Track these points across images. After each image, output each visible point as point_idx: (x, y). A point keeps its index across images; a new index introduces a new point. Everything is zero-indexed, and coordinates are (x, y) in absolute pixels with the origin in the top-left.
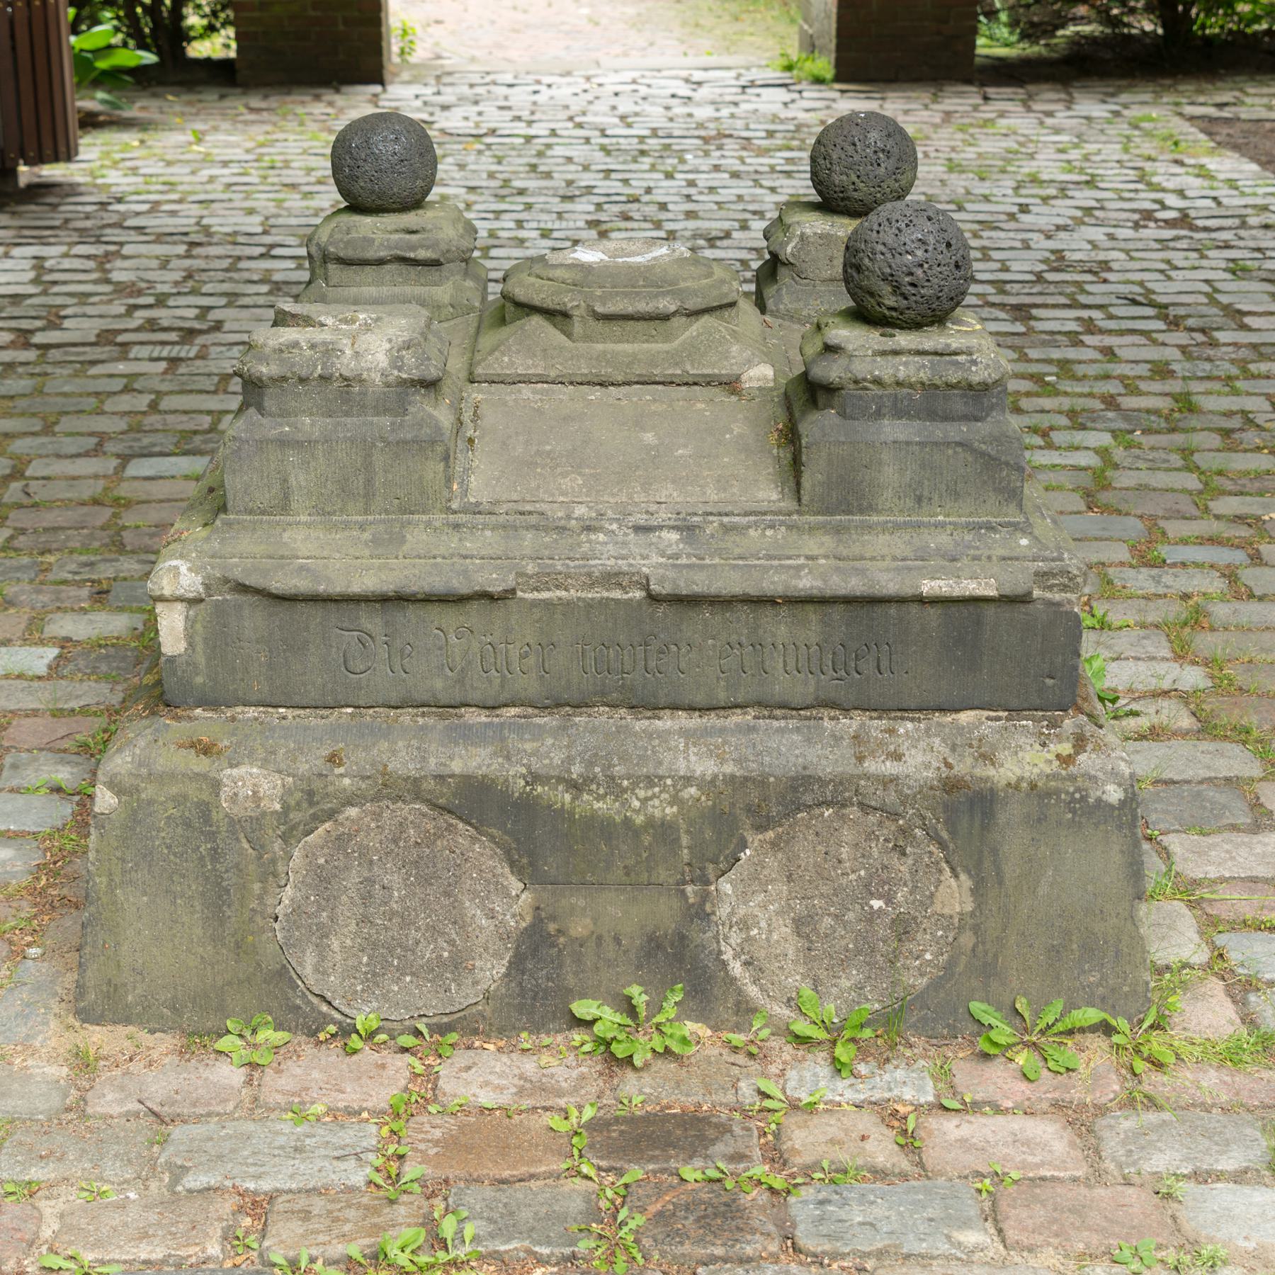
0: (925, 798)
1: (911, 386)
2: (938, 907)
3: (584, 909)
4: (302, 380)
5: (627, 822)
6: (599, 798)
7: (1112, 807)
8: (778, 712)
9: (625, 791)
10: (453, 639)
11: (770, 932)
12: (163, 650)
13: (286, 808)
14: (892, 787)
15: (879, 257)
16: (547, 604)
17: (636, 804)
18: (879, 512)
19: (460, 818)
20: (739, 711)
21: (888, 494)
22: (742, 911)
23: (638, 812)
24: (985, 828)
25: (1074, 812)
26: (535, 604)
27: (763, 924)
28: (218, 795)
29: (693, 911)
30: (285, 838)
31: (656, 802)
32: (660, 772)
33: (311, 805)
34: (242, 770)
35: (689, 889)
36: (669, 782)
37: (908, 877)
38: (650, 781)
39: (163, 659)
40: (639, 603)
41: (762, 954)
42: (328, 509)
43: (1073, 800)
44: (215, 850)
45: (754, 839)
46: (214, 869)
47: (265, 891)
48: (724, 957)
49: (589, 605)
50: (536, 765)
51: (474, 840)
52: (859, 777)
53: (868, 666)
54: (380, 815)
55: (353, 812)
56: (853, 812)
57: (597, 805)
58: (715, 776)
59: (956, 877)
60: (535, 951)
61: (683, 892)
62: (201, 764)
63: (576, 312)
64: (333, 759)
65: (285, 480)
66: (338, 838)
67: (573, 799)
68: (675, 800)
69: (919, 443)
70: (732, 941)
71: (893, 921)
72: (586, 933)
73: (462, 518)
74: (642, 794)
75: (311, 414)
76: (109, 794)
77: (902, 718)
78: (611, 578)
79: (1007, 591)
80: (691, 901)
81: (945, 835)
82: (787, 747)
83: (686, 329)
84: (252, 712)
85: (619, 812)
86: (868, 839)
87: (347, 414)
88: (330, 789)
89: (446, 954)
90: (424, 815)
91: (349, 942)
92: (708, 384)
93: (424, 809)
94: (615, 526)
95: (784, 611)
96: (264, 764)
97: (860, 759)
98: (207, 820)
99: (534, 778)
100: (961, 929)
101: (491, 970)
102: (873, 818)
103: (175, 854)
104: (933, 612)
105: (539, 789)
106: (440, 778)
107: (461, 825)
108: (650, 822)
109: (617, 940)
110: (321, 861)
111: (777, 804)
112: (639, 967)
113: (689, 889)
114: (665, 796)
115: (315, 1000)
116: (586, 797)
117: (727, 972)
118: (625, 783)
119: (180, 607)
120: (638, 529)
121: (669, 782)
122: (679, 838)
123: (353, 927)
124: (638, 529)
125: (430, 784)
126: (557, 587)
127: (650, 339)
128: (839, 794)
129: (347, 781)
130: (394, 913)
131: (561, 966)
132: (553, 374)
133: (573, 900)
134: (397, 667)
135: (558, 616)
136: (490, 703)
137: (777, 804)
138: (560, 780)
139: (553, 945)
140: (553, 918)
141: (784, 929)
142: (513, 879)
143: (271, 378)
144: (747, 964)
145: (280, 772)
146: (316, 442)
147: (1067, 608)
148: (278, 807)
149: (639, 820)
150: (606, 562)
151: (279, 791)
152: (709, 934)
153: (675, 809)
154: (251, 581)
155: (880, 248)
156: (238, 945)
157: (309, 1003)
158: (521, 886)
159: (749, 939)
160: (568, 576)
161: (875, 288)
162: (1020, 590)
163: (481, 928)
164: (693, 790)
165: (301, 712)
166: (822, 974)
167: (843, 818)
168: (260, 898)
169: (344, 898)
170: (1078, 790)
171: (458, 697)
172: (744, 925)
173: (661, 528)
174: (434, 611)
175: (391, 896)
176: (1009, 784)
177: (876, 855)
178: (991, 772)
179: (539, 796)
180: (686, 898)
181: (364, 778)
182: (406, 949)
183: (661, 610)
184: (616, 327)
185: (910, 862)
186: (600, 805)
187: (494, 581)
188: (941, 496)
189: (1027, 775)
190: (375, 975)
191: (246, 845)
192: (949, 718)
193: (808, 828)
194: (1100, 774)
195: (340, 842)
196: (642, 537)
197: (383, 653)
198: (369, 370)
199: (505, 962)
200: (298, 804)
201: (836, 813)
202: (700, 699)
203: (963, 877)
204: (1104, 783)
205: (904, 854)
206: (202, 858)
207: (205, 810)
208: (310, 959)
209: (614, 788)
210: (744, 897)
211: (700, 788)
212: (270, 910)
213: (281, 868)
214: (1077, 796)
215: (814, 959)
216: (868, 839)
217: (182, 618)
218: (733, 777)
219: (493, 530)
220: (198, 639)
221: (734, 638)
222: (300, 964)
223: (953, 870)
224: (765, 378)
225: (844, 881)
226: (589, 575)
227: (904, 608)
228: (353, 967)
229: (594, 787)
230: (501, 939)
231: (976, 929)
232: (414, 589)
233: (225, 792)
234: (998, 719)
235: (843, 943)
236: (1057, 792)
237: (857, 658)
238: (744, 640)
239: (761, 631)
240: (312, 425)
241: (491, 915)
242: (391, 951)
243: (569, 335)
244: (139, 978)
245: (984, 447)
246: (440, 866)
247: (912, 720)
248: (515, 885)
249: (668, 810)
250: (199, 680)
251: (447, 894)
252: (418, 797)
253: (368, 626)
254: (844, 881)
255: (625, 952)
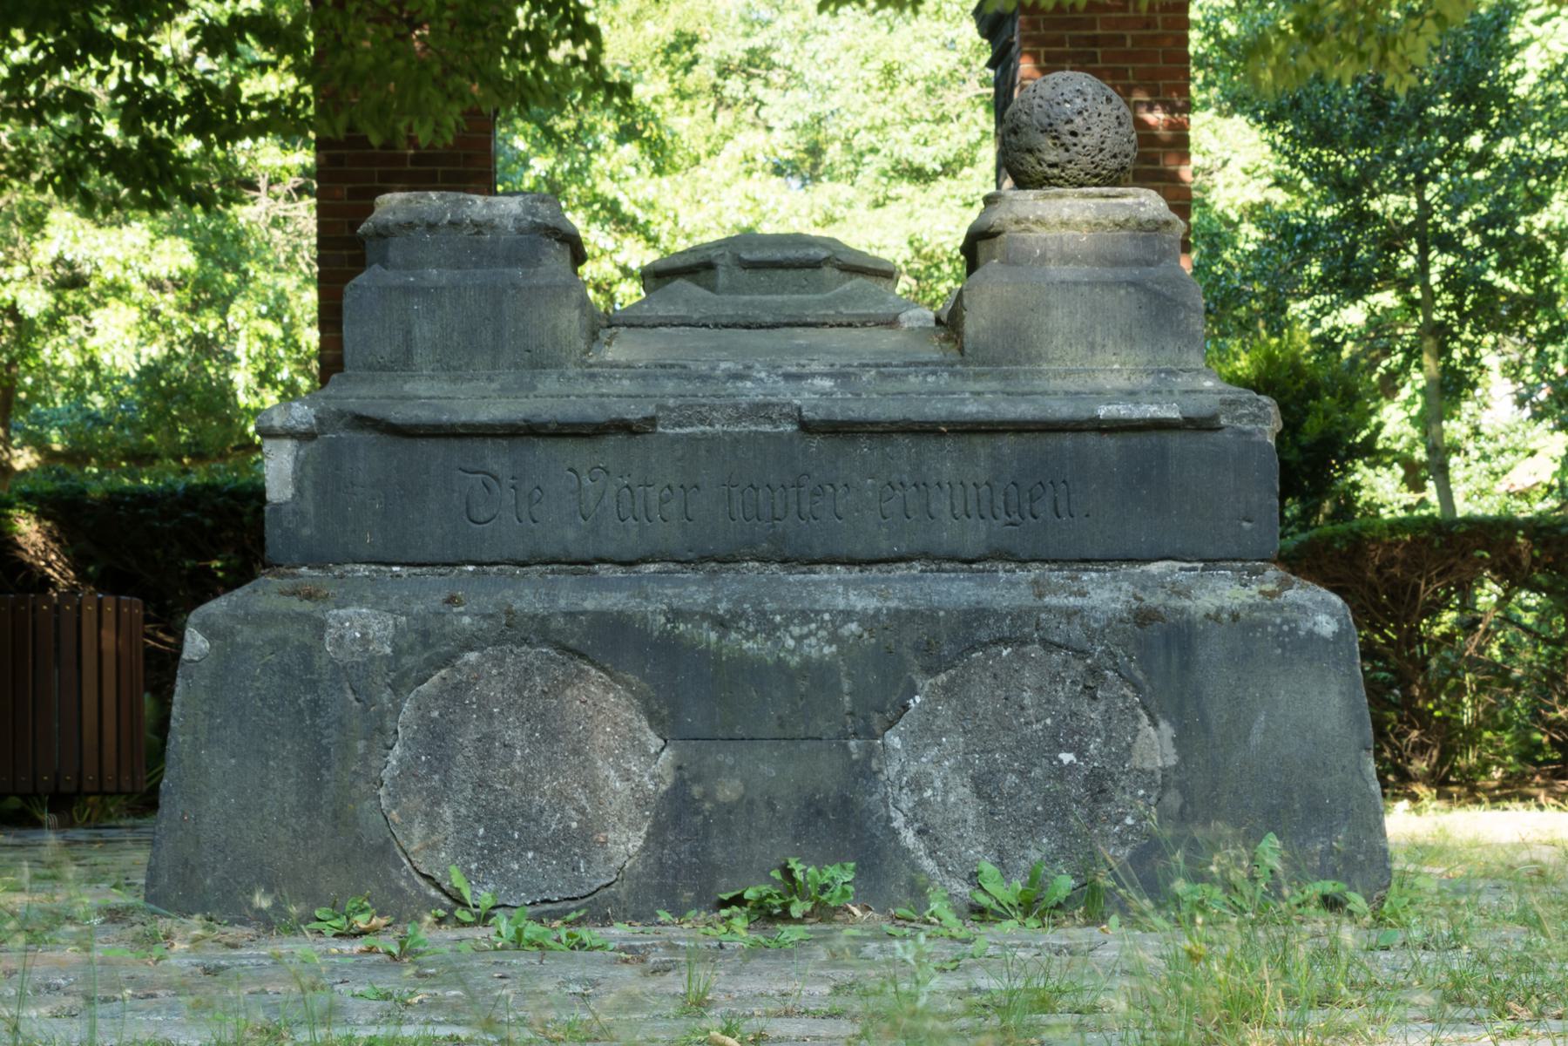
0: (1114, 632)
1: (1077, 226)
2: (1136, 761)
3: (732, 768)
4: (431, 227)
5: (781, 664)
6: (750, 636)
7: (1325, 640)
8: (947, 566)
9: (776, 627)
10: (586, 482)
11: (946, 793)
12: (269, 496)
13: (398, 652)
14: (1077, 620)
15: (1036, 109)
16: (691, 438)
17: (791, 643)
18: (1049, 362)
19: (592, 663)
20: (903, 565)
21: (1058, 340)
22: (913, 768)
23: (792, 652)
24: (1186, 666)
25: (1283, 646)
26: (677, 439)
27: (938, 784)
28: (322, 638)
29: (857, 769)
30: (395, 687)
31: (813, 641)
32: (817, 607)
33: (429, 648)
34: (351, 611)
35: (852, 743)
36: (827, 617)
37: (1100, 725)
38: (805, 616)
39: (267, 508)
40: (791, 436)
41: (938, 820)
42: (454, 363)
43: (1281, 633)
44: (316, 702)
45: (925, 683)
46: (313, 725)
47: (369, 750)
48: (895, 824)
49: (736, 440)
50: (676, 603)
51: (607, 689)
52: (1040, 610)
53: (1044, 508)
54: (503, 660)
55: (472, 656)
56: (1034, 651)
57: (747, 645)
58: (878, 611)
59: (1155, 725)
60: (676, 819)
61: (846, 747)
62: (307, 606)
63: (719, 261)
64: (451, 601)
65: (409, 332)
66: (455, 687)
67: (720, 638)
68: (834, 638)
69: (1088, 283)
70: (903, 806)
71: (1086, 778)
72: (735, 797)
73: (595, 370)
74: (796, 631)
75: (438, 266)
76: (199, 638)
77: (1086, 570)
78: (759, 411)
79: (1192, 412)
80: (855, 757)
81: (1139, 675)
82: (957, 590)
83: (840, 283)
84: (362, 570)
85: (771, 653)
86: (1053, 681)
87: (477, 265)
88: (448, 629)
89: (574, 825)
90: (552, 660)
91: (463, 811)
92: (864, 325)
93: (553, 653)
94: (763, 375)
95: (949, 443)
96: (374, 605)
97: (1041, 596)
98: (308, 664)
99: (676, 615)
100: (1165, 787)
101: (626, 844)
102: (1056, 657)
103: (270, 708)
104: (1111, 442)
105: (682, 627)
106: (571, 615)
107: (593, 672)
108: (807, 663)
109: (770, 805)
110: (435, 714)
111: (951, 644)
112: (797, 838)
113: (852, 743)
114: (823, 633)
115: (422, 883)
116: (733, 635)
117: (898, 843)
118: (778, 618)
119: (289, 444)
120: (788, 377)
121: (827, 617)
122: (839, 683)
123: (469, 793)
124: (788, 377)
125: (559, 622)
126: (702, 422)
127: (801, 289)
128: (1017, 631)
129: (466, 620)
130: (516, 775)
131: (707, 837)
132: (696, 316)
133: (720, 757)
134: (525, 516)
135: (702, 453)
136: (627, 557)
137: (951, 644)
138: (705, 616)
139: (697, 812)
140: (697, 779)
141: (961, 789)
142: (651, 734)
143: (398, 225)
144: (920, 832)
145: (392, 611)
146: (443, 288)
147: (1259, 437)
148: (388, 650)
149: (794, 661)
150: (750, 392)
151: (391, 631)
152: (876, 797)
153: (834, 648)
154: (369, 412)
155: (1037, 101)
156: (336, 816)
157: (416, 884)
158: (661, 742)
159: (922, 803)
160: (713, 408)
161: (1033, 143)
162: (1206, 412)
163: (615, 792)
164: (854, 626)
165: (417, 570)
166: (1009, 844)
167: (1024, 658)
168: (364, 758)
169: (460, 757)
170: (1286, 621)
171: (590, 551)
172: (917, 785)
173: (813, 375)
174: (568, 446)
175: (513, 756)
176: (1207, 616)
177: (1063, 700)
178: (1187, 603)
179: (681, 635)
180: (849, 754)
181: (485, 617)
182: (528, 818)
183: (816, 442)
184: (762, 277)
185: (1102, 708)
186: (750, 644)
187: (633, 412)
188: (1115, 343)
189: (1227, 604)
190: (492, 850)
191: (352, 698)
192: (1138, 569)
193: (985, 669)
194: (1309, 604)
195: (456, 692)
196: (793, 385)
197: (509, 497)
198: (501, 216)
199: (642, 833)
200: (412, 647)
201: (1015, 652)
202: (859, 549)
203: (1163, 725)
204: (1314, 612)
205: (1094, 698)
206: (300, 712)
207: (307, 654)
208: (418, 831)
209: (767, 627)
210: (915, 752)
211: (861, 623)
212: (374, 774)
213: (389, 724)
214: (1286, 628)
215: (997, 825)
216: (1053, 681)
217: (290, 459)
218: (898, 611)
219: (631, 379)
220: (307, 483)
221: (895, 478)
222: (407, 837)
223: (1151, 717)
224: (925, 318)
225: (1028, 731)
226: (736, 406)
227: (1081, 437)
228: (467, 841)
229: (743, 624)
230: (638, 805)
231: (1183, 788)
232: (546, 417)
233: (330, 635)
234: (1194, 569)
235: (1030, 805)
236: (1262, 624)
237: (1032, 500)
238: (906, 478)
239: (924, 469)
240: (440, 274)
241: (626, 776)
242: (511, 821)
243: (712, 288)
244: (220, 856)
245: (1157, 287)
246: (569, 719)
247: (1097, 571)
248: (654, 742)
249: (826, 650)
250: (306, 532)
251: (576, 752)
252: (546, 640)
253: (493, 465)
254: (1028, 731)
255: (781, 820)
